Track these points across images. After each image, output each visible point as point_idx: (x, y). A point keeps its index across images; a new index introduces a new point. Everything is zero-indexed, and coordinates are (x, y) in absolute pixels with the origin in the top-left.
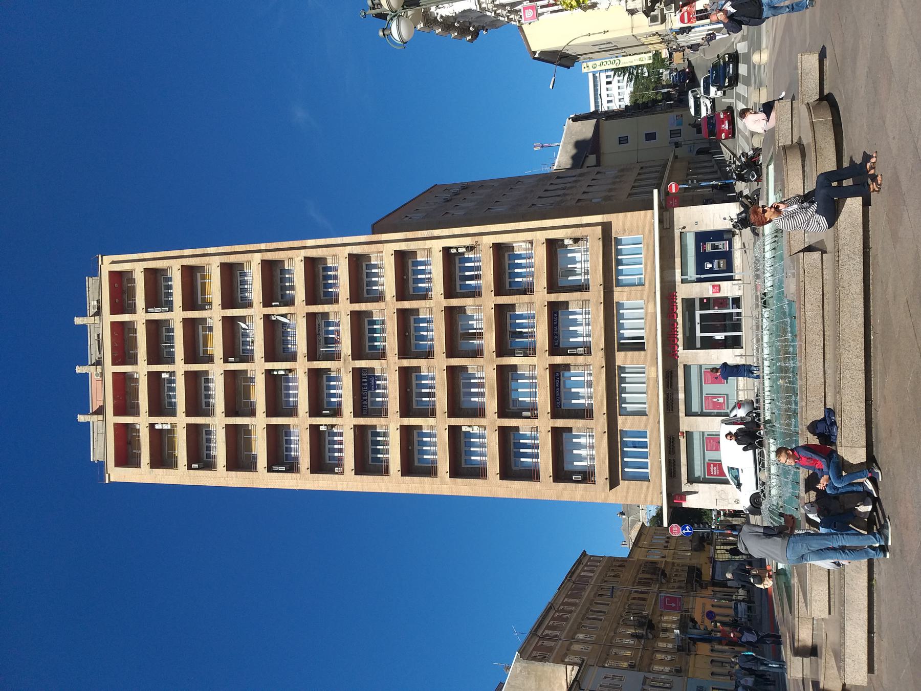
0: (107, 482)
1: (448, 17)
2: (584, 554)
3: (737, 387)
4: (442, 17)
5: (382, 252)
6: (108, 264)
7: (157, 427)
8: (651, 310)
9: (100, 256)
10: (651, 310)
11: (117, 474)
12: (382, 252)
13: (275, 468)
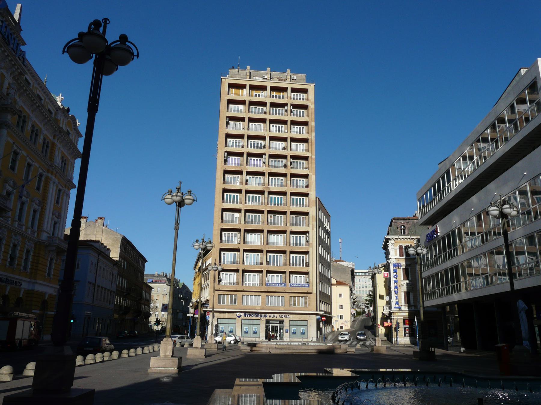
0: (222, 77)
1: (388, 246)
2: (147, 261)
3: (245, 337)
4: (388, 244)
5: (309, 207)
6: (311, 88)
7: (264, 156)
8: (281, 309)
9: (314, 84)
10: (281, 309)
11: (226, 81)
12: (309, 207)
13: (226, 153)
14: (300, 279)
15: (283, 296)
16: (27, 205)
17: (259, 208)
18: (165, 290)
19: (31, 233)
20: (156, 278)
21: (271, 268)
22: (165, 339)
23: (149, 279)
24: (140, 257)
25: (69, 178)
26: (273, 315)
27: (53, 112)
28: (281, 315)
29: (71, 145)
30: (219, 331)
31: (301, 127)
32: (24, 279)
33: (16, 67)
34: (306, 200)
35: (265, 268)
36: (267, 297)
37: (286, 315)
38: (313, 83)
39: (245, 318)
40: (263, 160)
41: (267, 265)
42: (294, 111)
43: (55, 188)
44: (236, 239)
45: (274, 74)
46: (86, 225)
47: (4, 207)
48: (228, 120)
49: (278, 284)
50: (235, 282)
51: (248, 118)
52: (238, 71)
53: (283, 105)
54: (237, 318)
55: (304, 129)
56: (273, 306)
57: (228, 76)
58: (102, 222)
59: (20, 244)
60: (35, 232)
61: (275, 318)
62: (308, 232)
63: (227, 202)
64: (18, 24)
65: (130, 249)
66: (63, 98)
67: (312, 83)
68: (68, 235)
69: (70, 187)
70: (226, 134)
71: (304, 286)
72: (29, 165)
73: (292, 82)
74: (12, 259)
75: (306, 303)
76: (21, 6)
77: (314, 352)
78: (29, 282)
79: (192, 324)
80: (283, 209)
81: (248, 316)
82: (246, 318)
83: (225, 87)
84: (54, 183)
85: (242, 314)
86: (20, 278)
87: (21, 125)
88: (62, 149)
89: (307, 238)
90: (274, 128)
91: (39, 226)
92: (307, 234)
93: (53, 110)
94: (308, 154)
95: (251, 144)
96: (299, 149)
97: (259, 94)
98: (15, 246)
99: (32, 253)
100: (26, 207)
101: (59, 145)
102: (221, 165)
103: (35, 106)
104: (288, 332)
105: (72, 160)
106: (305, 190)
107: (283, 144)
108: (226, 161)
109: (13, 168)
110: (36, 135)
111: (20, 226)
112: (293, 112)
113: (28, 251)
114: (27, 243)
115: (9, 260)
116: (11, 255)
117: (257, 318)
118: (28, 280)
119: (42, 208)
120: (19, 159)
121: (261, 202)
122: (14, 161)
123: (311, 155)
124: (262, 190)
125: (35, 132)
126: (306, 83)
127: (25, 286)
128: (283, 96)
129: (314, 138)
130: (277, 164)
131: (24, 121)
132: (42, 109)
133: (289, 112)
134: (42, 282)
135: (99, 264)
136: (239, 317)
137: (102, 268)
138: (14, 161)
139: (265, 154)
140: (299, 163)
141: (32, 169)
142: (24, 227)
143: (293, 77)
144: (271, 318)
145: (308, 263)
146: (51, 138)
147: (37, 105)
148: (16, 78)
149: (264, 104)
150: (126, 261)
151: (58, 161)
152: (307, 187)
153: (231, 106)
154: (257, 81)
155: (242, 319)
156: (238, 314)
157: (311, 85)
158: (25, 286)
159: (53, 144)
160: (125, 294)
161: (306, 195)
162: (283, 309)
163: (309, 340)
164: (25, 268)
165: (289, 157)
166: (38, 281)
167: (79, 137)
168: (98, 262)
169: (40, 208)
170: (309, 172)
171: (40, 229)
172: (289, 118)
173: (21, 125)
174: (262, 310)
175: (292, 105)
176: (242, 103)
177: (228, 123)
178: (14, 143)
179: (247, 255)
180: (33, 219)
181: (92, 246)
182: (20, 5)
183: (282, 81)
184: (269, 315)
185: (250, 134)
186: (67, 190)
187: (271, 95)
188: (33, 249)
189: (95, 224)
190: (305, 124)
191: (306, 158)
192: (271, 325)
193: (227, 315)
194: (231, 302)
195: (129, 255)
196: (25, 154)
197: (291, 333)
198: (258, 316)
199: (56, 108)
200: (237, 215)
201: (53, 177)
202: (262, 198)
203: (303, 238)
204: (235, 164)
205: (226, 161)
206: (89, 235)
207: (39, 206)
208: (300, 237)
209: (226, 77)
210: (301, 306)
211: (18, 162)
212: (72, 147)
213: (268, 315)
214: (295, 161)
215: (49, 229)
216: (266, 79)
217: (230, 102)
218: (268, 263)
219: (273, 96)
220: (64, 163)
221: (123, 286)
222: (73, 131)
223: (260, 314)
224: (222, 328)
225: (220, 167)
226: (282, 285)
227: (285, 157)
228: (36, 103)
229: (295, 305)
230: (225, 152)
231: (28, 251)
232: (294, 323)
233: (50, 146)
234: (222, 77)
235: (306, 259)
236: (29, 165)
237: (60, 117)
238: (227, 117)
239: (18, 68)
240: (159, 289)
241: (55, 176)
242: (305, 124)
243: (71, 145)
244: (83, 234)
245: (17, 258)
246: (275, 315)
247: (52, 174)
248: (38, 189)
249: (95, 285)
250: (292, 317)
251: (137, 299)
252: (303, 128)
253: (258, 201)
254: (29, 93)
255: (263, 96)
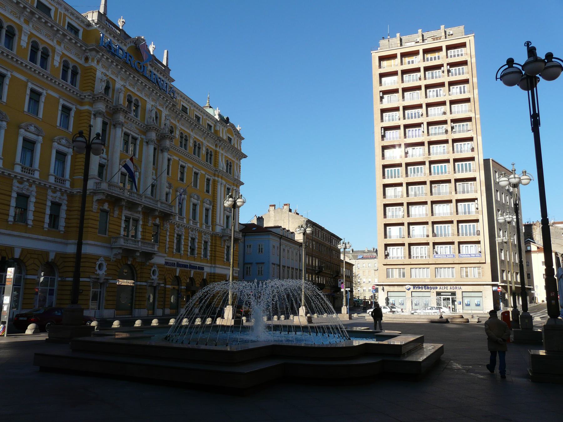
0: (372, 52)
6: (470, 40)
7: (422, 125)
13: (383, 129)
14: (472, 249)
15: (454, 268)
16: (199, 206)
17: (421, 180)
18: (376, 265)
19: (205, 228)
20: (366, 254)
21: (437, 240)
22: (228, 306)
23: (359, 255)
24: (332, 236)
25: (237, 178)
26: (443, 287)
27: (213, 125)
28: (452, 287)
29: (232, 149)
30: (390, 303)
31: (462, 86)
32: (205, 264)
33: (169, 102)
34: (473, 164)
35: (431, 240)
36: (436, 269)
37: (457, 286)
38: (473, 33)
39: (414, 290)
40: (422, 129)
41: (433, 236)
42: (453, 69)
43: (223, 188)
44: (401, 213)
45: (426, 35)
46: (274, 212)
47: (170, 213)
48: (381, 95)
49: (447, 255)
50: (403, 255)
51: (402, 88)
52: (389, 41)
53: (439, 67)
54: (407, 291)
55: (466, 88)
56: (443, 277)
57: (379, 48)
58: (287, 208)
59: (197, 237)
60: (209, 227)
61: (446, 290)
62: (477, 199)
63: (388, 178)
64: (166, 67)
65: (319, 231)
66: (219, 111)
67: (471, 34)
68: (254, 224)
69: (238, 184)
70: (381, 109)
71: (475, 256)
72: (196, 174)
73: (450, 38)
74: (193, 250)
75: (479, 273)
76: (167, 51)
77: (425, 321)
78: (211, 267)
79: (350, 298)
80: (446, 178)
81: (418, 288)
82: (416, 290)
83: (376, 61)
84: (221, 184)
85: (412, 287)
86: (202, 264)
87: (184, 143)
88: (225, 154)
89: (477, 205)
90: (431, 94)
91: (212, 221)
92: (476, 201)
93: (212, 123)
94: (472, 115)
95: (408, 114)
96: (460, 111)
97: (412, 60)
98: (193, 239)
99: (209, 244)
100: (198, 208)
101: (221, 152)
102: (379, 141)
103: (193, 126)
104: (461, 304)
105: (236, 161)
106: (469, 155)
107: (442, 109)
108: (383, 137)
109: (182, 179)
110: (199, 148)
111: (195, 223)
112: (452, 71)
113: (206, 242)
114: (204, 236)
115: (189, 250)
116: (190, 247)
117: (427, 290)
118: (210, 265)
119: (213, 206)
120: (186, 171)
121: (423, 173)
122: (182, 173)
123: (476, 116)
124: (422, 160)
125: (197, 147)
126: (465, 35)
127: (207, 270)
128: (439, 57)
129: (478, 96)
130: (437, 131)
131: (186, 140)
132: (199, 127)
133: (446, 72)
134: (220, 266)
135: (281, 247)
136: (409, 289)
137: (286, 251)
138: (182, 173)
139: (423, 123)
140: (462, 126)
141: (199, 176)
142: (198, 224)
143: (449, 33)
144: (441, 290)
145: (478, 232)
146: (214, 147)
147: (194, 124)
148: (172, 109)
149: (417, 70)
150: (315, 241)
151: (222, 165)
152: (473, 150)
153: (384, 79)
154: (409, 47)
155: (412, 292)
156: (406, 286)
157: (469, 37)
158: (207, 270)
159: (216, 152)
160: (317, 272)
161: (472, 159)
162: (454, 281)
163: (485, 312)
164: (205, 255)
165: (449, 122)
166: (217, 266)
167: (241, 140)
168: (280, 245)
169: (211, 206)
170: (474, 133)
171: (214, 224)
172: (446, 79)
173: (184, 143)
174: (431, 282)
175: (448, 64)
176: (395, 73)
177: (382, 98)
178: (179, 159)
179: (413, 228)
180: (207, 216)
181: (271, 232)
182: (166, 50)
183: (437, 40)
184: (440, 286)
185: (405, 105)
186: (235, 188)
187: (426, 59)
188: (210, 240)
189: (282, 211)
190: (466, 81)
191: (469, 119)
192: (442, 297)
193: (396, 289)
194: (400, 276)
195: (317, 236)
196: (191, 166)
197: (464, 305)
198: (428, 288)
199: (215, 121)
200: (399, 189)
201: (220, 180)
202: (424, 168)
203: (473, 205)
204: (393, 138)
205: (383, 137)
206: (278, 221)
207: (210, 205)
208: (469, 205)
209: (378, 50)
210: (474, 277)
211: (185, 173)
212: (234, 150)
213: (439, 287)
214: (457, 124)
215: (222, 222)
216: (418, 42)
217: (382, 75)
218: (434, 235)
219: (428, 59)
220: (230, 166)
221: (314, 265)
222: (235, 136)
223: (429, 287)
224: (393, 301)
225: (378, 143)
226: (451, 256)
227: (445, 122)
228: (193, 123)
229: (467, 276)
230: (382, 128)
231: (206, 242)
232: (468, 294)
233: (213, 154)
234: (372, 52)
235: (477, 227)
236: (196, 174)
237: (219, 127)
238: (380, 91)
239: (170, 102)
240: (370, 265)
241: (222, 178)
242: (466, 81)
243: (232, 149)
244: (273, 220)
245: (196, 248)
246: (446, 287)
247: (218, 177)
248: (208, 191)
249: (279, 266)
250: (464, 288)
251: (334, 276)
252: (464, 87)
253: (416, 173)
254: (185, 117)
255: (418, 62)
